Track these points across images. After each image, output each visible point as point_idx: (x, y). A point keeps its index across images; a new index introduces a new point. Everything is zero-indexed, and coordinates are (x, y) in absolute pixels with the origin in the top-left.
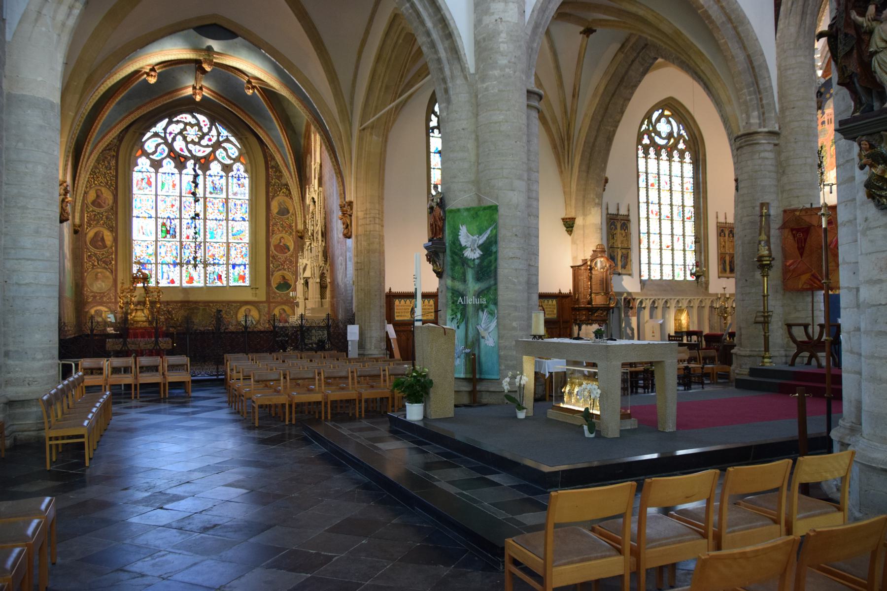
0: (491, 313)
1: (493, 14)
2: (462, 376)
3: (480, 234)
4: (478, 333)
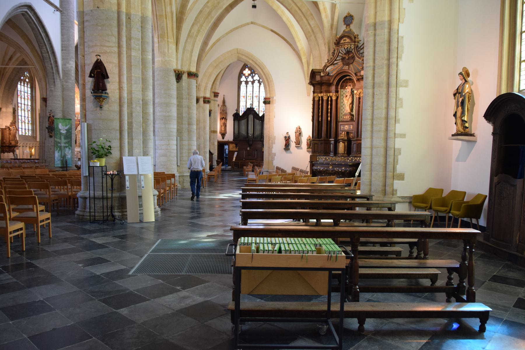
0: (69, 149)
1: (70, 64)
2: (60, 166)
3: (66, 126)
4: (65, 154)
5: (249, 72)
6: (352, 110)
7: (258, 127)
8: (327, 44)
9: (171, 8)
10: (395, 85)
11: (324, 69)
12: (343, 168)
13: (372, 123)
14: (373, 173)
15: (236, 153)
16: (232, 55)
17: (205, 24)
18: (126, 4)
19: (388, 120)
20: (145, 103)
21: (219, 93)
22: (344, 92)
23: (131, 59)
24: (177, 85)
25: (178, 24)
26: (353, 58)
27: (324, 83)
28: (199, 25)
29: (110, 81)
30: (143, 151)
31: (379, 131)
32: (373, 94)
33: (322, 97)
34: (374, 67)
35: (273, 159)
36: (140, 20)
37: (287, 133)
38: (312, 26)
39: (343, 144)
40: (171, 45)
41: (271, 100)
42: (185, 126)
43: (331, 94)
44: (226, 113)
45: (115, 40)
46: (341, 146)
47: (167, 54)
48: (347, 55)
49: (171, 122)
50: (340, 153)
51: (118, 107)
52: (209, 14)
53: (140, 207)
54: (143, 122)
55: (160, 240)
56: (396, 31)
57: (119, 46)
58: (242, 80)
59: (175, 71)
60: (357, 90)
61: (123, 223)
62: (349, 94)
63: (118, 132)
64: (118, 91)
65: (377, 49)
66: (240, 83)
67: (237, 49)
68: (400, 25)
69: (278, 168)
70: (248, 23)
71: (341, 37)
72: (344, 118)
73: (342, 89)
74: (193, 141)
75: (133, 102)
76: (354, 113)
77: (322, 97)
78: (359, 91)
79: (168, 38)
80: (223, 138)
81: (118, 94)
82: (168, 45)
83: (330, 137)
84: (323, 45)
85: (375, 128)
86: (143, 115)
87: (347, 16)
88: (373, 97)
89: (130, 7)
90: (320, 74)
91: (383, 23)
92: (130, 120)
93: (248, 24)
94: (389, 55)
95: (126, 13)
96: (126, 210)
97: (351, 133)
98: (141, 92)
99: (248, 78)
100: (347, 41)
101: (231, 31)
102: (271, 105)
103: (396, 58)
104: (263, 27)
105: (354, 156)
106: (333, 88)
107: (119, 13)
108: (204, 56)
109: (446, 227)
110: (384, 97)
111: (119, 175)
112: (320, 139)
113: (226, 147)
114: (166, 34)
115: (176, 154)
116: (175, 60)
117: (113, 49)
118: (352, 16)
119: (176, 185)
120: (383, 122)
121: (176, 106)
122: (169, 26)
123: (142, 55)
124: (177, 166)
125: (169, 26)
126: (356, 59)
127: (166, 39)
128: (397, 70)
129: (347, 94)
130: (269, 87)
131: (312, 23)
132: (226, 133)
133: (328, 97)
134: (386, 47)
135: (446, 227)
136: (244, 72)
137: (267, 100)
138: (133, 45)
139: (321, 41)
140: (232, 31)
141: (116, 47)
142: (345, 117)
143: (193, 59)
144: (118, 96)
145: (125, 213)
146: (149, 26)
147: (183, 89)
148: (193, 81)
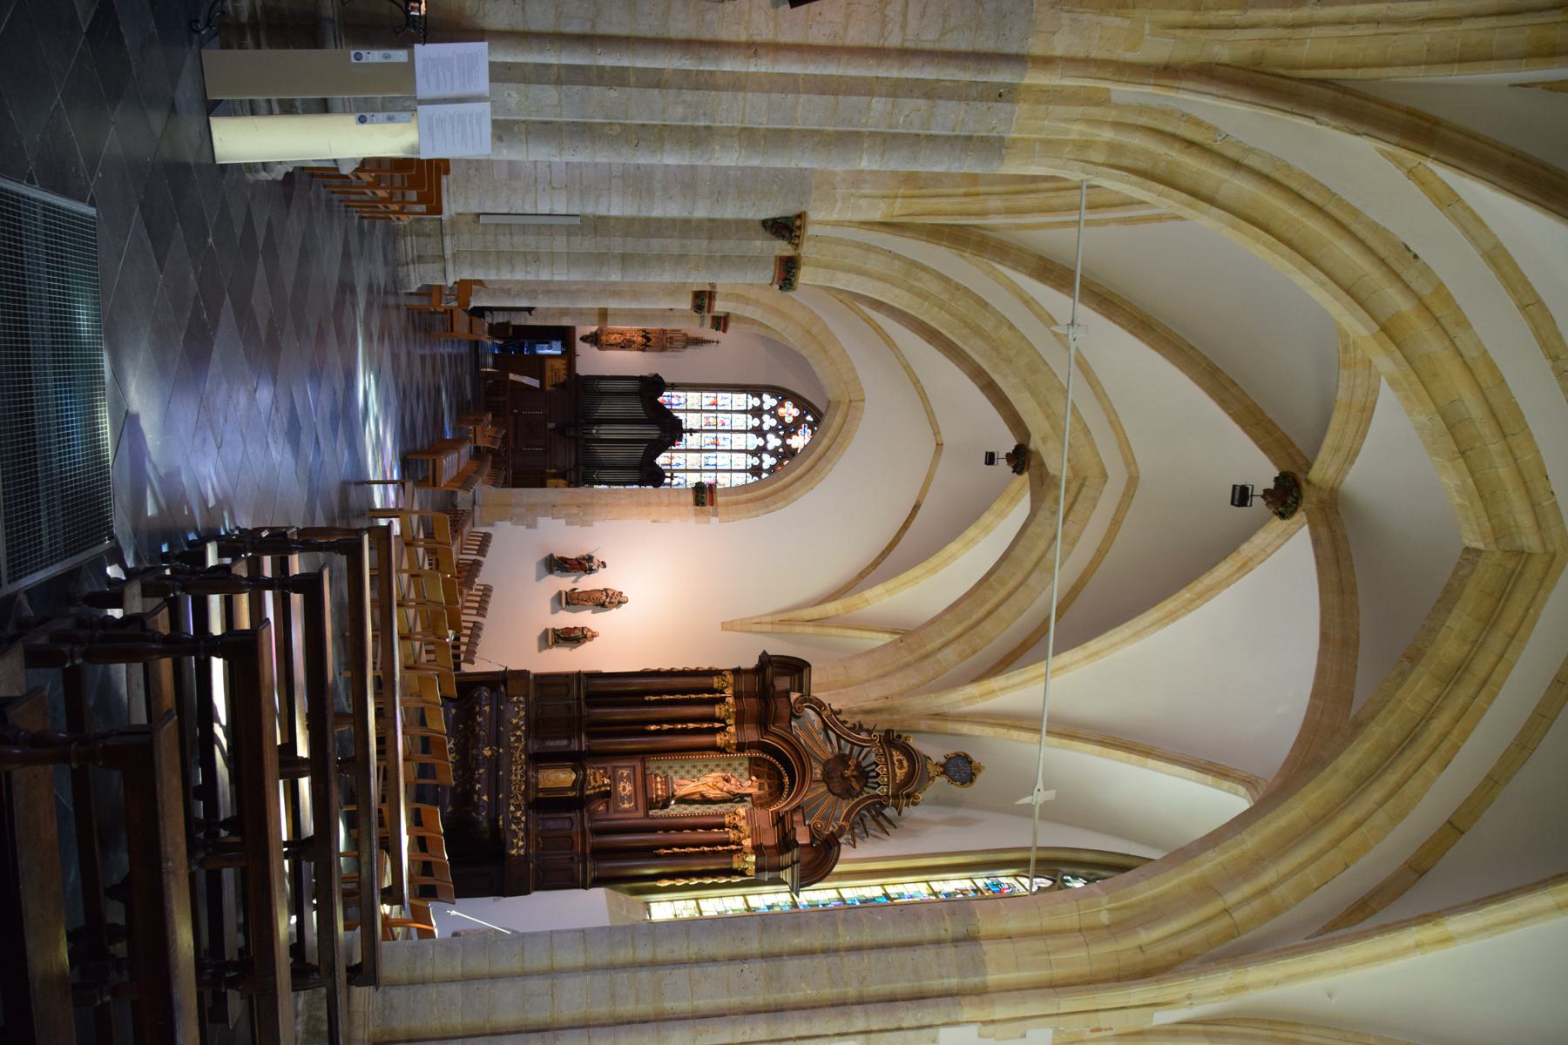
5: (789, 420)
6: (683, 800)
7: (620, 455)
8: (889, 703)
9: (998, 212)
10: (774, 1037)
11: (811, 701)
12: (485, 798)
13: (642, 965)
14: (455, 990)
15: (535, 383)
16: (845, 383)
17: (947, 316)
18: (1048, 86)
19: (654, 1024)
20: (697, 137)
21: (724, 331)
22: (741, 770)
23: (859, 95)
24: (753, 221)
25: (947, 230)
26: (847, 793)
27: (767, 705)
28: (945, 297)
29: (781, 9)
30: (515, 122)
31: (613, 997)
32: (745, 958)
33: (722, 700)
34: (836, 951)
35: (517, 519)
36: (994, 134)
37: (604, 564)
38: (940, 656)
39: (569, 785)
40: (882, 205)
41: (708, 508)
42: (618, 245)
43: (732, 729)
44: (663, 349)
45: (929, 38)
46: (563, 778)
47: (854, 191)
48: (855, 773)
49: (630, 198)
50: (540, 776)
51: (683, 36)
52: (978, 332)
53: (280, 102)
54: (626, 125)
55: (92, 211)
56: (954, 1018)
57: (905, 54)
58: (766, 397)
59: (799, 216)
60: (749, 818)
61: (198, 32)
62: (732, 787)
63: (585, 28)
64: (743, 38)
65: (893, 956)
66: (756, 391)
67: (863, 400)
68: (974, 1028)
69: (486, 539)
70: (939, 432)
71: (909, 753)
72: (656, 776)
73: (750, 764)
74: (568, 271)
75: (701, 92)
76: (674, 809)
77: (722, 700)
78: (742, 824)
79: (904, 197)
80: (584, 339)
81: (733, 38)
82: (884, 197)
83: (591, 736)
84: (886, 693)
85: (623, 977)
86: (655, 126)
87: (971, 762)
88: (732, 959)
89: (1038, 102)
90: (796, 688)
91: (979, 966)
92: (633, 80)
93: (936, 433)
94: (877, 1002)
95: (1019, 84)
96: (263, 41)
97: (607, 803)
98: (740, 125)
99: (772, 416)
100: (897, 771)
101: (916, 382)
102: (692, 508)
103: (868, 1029)
104: (929, 478)
105: (531, 826)
106: (752, 735)
107: (1018, 60)
108: (841, 297)
110: (733, 1000)
111: (407, 25)
112: (583, 703)
113: (556, 350)
114: (917, 192)
115: (520, 212)
116: (835, 216)
117: (897, 29)
118: (971, 781)
119: (401, 217)
120: (645, 1008)
121: (685, 214)
122: (943, 204)
123: (871, 134)
124: (478, 215)
125: (943, 204)
126: (844, 802)
127: (901, 191)
128: (826, 1036)
129: (733, 781)
130: (747, 502)
131: (950, 654)
132: (599, 349)
133: (722, 721)
134: (901, 986)
136: (788, 405)
137: (707, 496)
138: (909, 104)
139: (896, 684)
140: (915, 384)
141: (904, 41)
142: (659, 779)
143: (840, 275)
144: (724, 35)
145: (249, 41)
146: (970, 165)
147: (740, 239)
148: (768, 274)
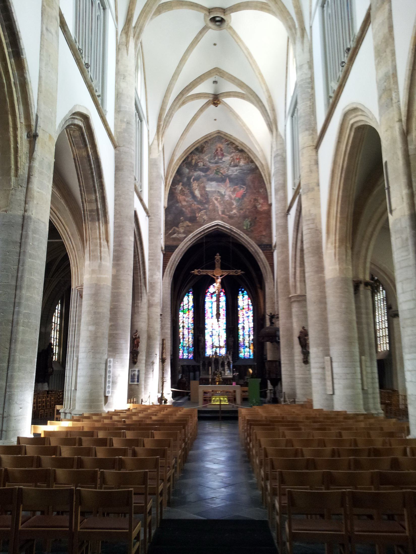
1: (157, 275)
109: (50, 241)
135: (50, 241)
